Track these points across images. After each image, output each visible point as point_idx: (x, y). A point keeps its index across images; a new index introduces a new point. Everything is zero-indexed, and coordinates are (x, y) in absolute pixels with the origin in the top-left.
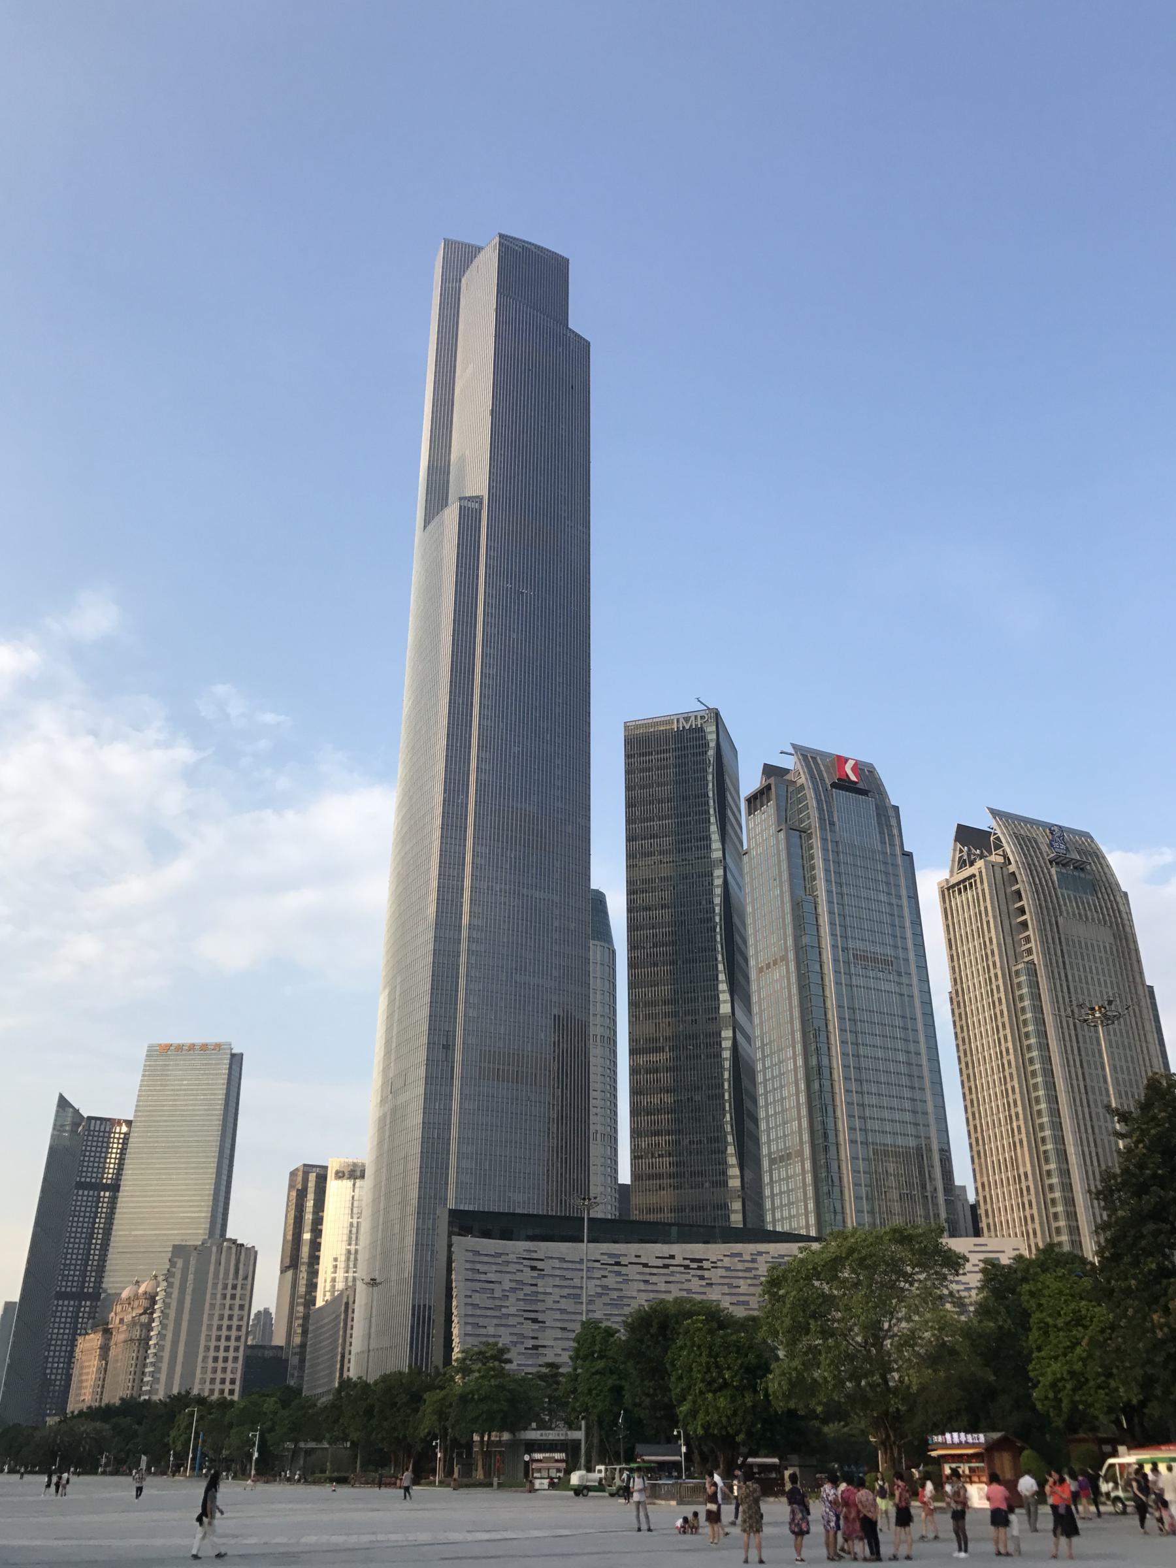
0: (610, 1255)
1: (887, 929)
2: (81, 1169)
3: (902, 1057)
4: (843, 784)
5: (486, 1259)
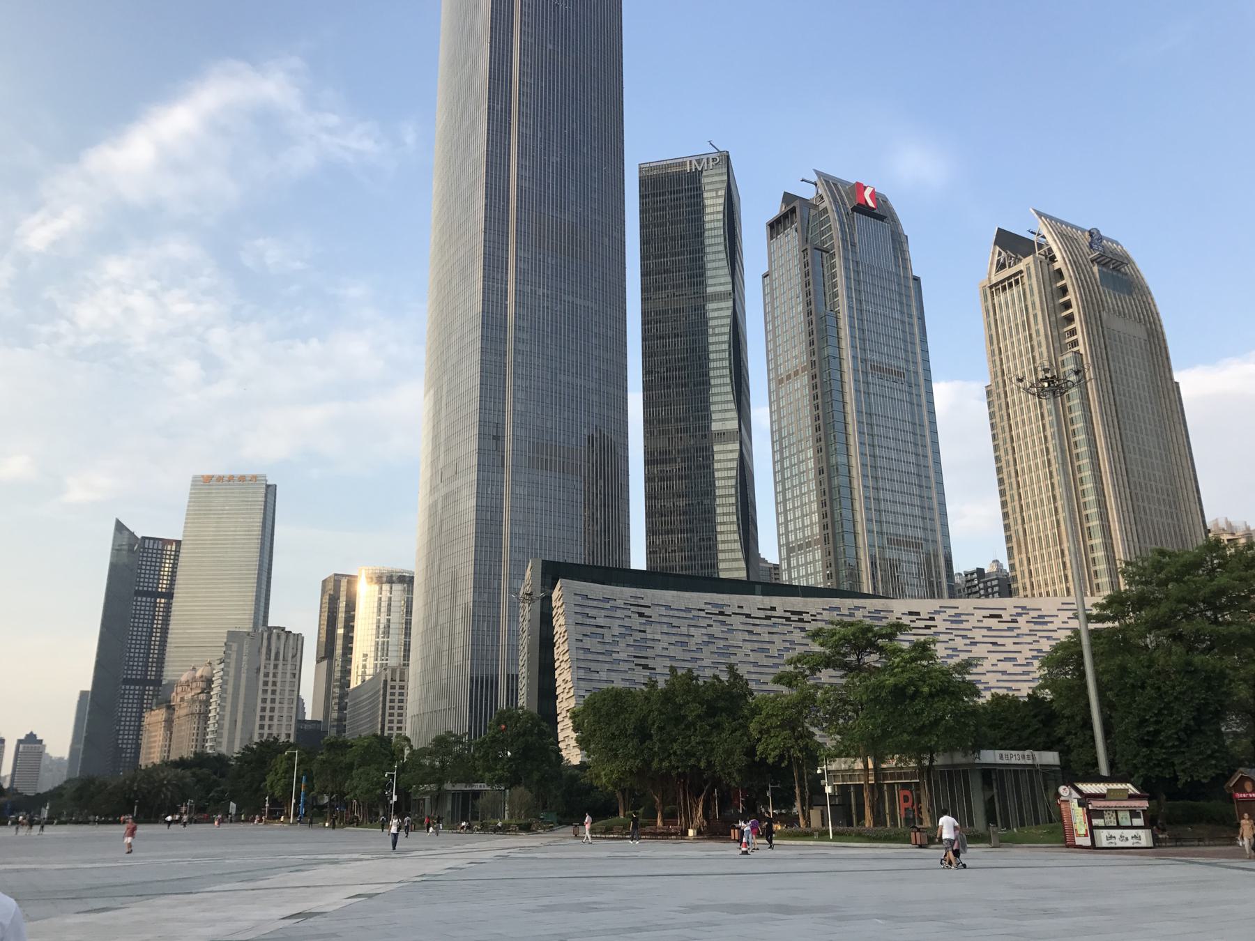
0: (716, 605)
1: (901, 344)
2: (140, 582)
3: (912, 459)
4: (862, 209)
5: (595, 604)
